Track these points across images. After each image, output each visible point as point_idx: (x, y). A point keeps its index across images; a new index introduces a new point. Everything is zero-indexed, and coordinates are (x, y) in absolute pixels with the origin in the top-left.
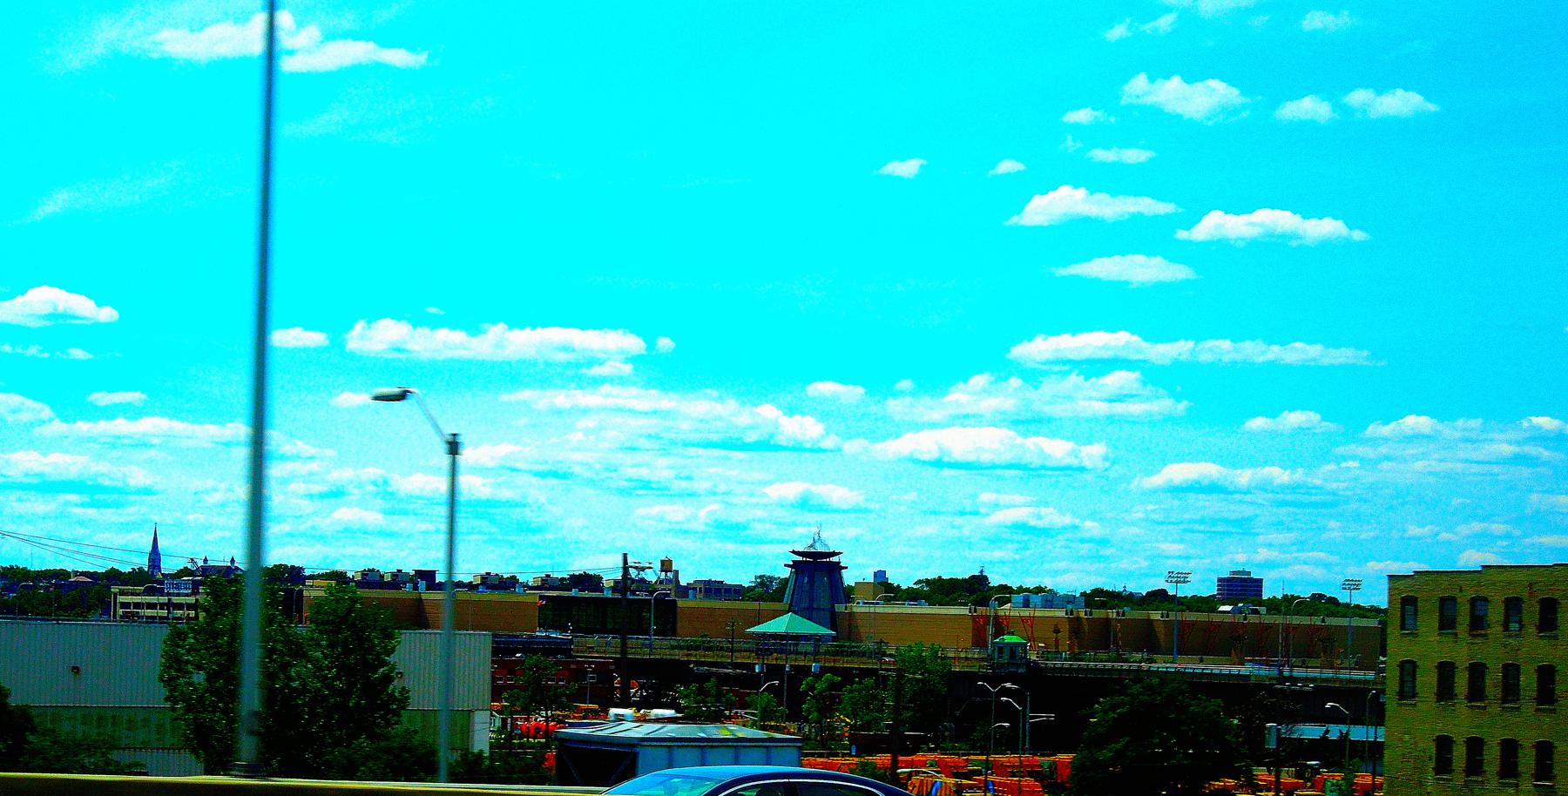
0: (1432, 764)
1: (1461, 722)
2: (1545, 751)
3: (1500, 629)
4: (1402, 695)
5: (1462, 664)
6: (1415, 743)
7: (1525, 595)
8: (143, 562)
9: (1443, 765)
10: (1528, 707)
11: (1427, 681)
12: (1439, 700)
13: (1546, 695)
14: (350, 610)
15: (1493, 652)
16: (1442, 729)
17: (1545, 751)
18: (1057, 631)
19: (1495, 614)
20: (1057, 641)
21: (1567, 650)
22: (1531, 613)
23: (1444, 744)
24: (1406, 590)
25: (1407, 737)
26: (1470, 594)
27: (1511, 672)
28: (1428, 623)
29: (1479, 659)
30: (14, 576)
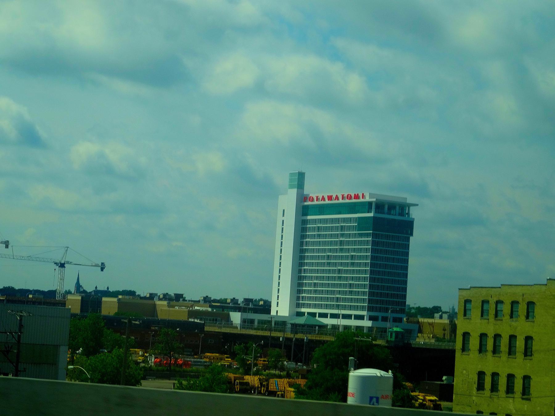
0: (476, 386)
1: (490, 364)
2: (526, 379)
3: (509, 317)
4: (463, 350)
5: (491, 335)
6: (468, 375)
7: (520, 300)
8: (19, 369)
9: (481, 387)
10: (504, 356)
11: (474, 343)
12: (455, 350)
13: (528, 352)
14: (160, 354)
15: (505, 328)
16: (480, 368)
17: (526, 379)
18: (444, 330)
19: (506, 309)
20: (444, 335)
21: (540, 328)
22: (522, 309)
23: (481, 375)
24: (466, 295)
25: (465, 372)
26: (495, 299)
27: (497, 337)
28: (475, 313)
29: (499, 332)
30: (8, 292)
